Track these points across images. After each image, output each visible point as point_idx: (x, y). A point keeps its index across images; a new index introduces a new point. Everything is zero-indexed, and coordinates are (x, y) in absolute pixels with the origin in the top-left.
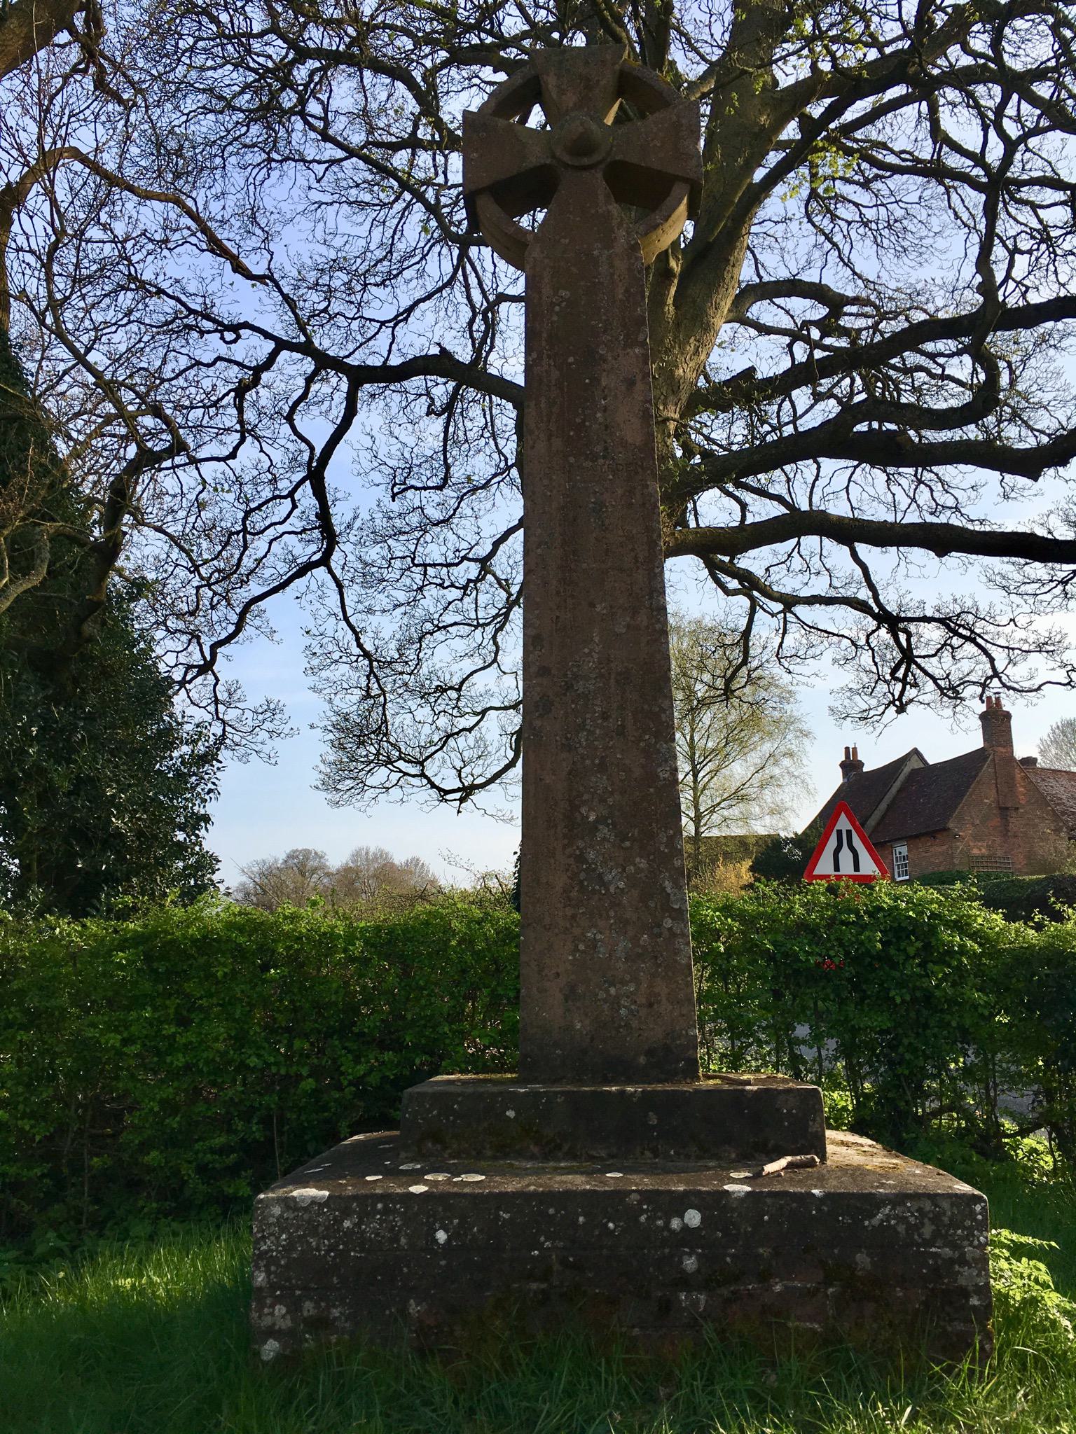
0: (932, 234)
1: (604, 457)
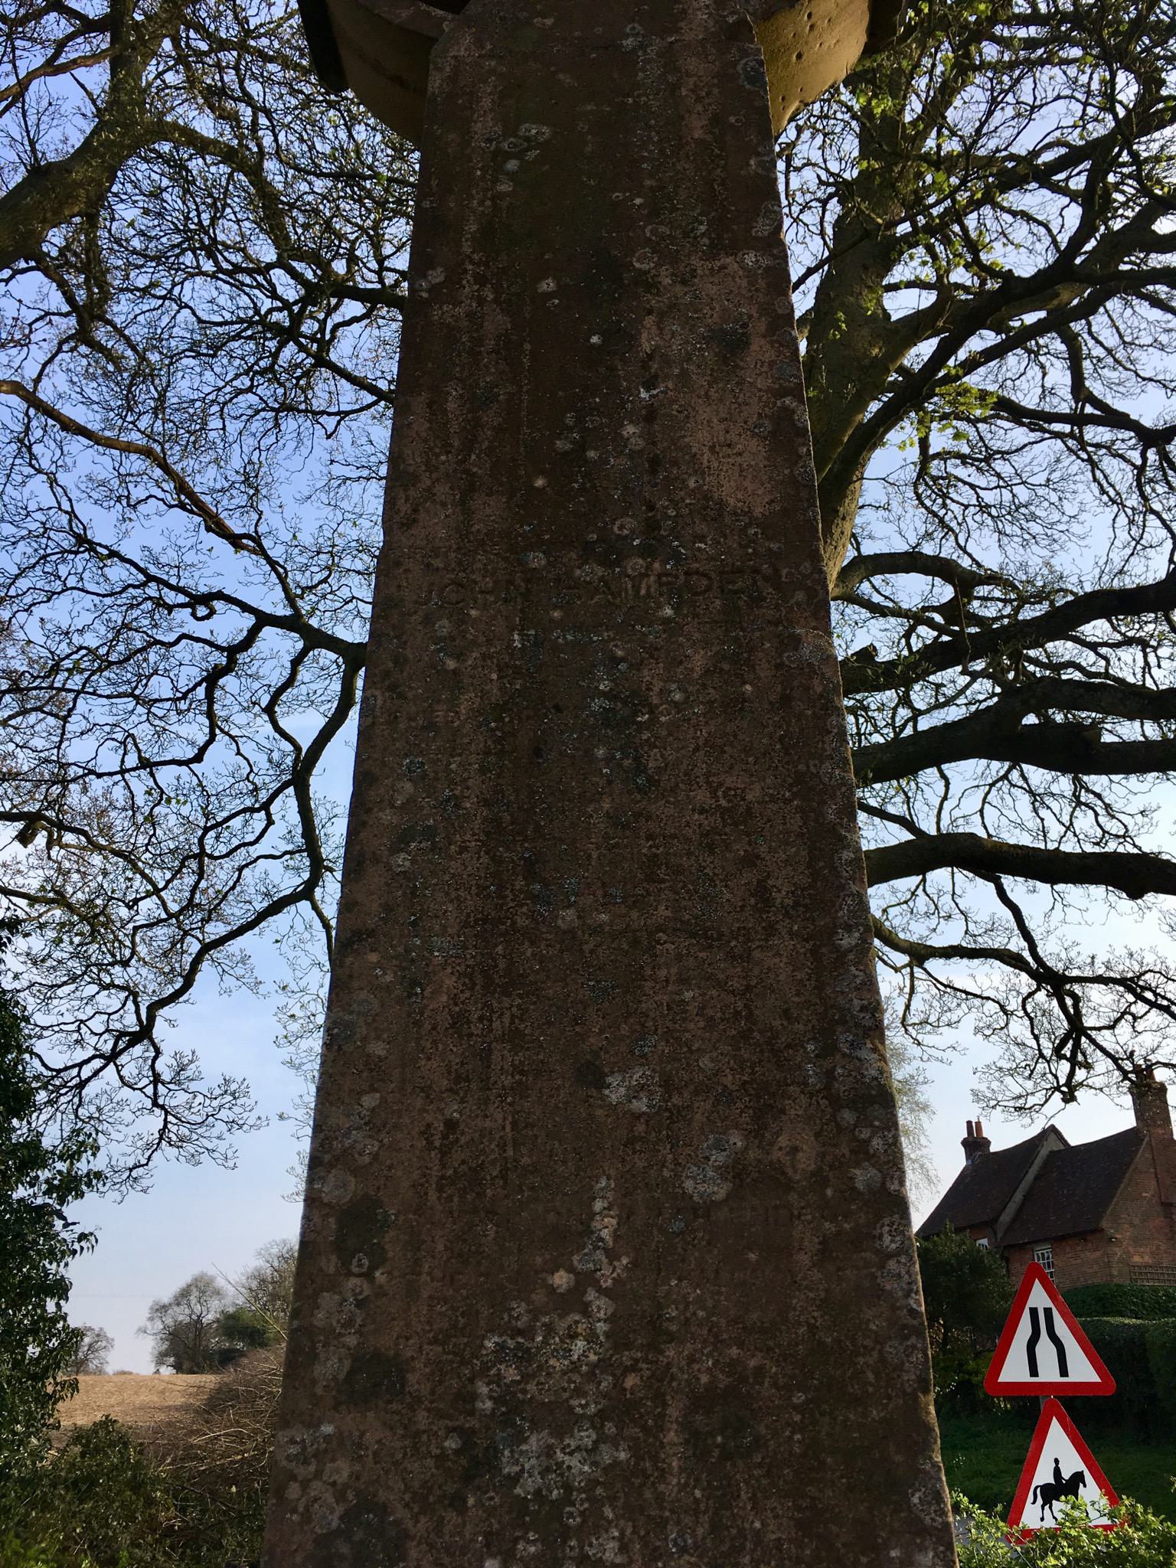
0: (1065, 519)
1: (646, 551)
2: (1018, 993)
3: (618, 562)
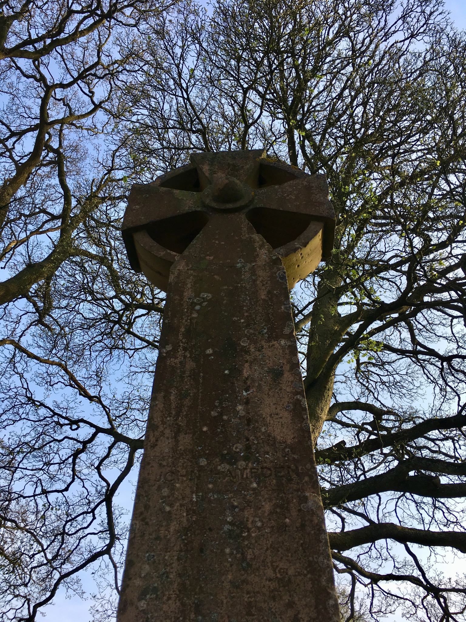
1: (246, 459)
2: (420, 596)
3: (235, 463)
